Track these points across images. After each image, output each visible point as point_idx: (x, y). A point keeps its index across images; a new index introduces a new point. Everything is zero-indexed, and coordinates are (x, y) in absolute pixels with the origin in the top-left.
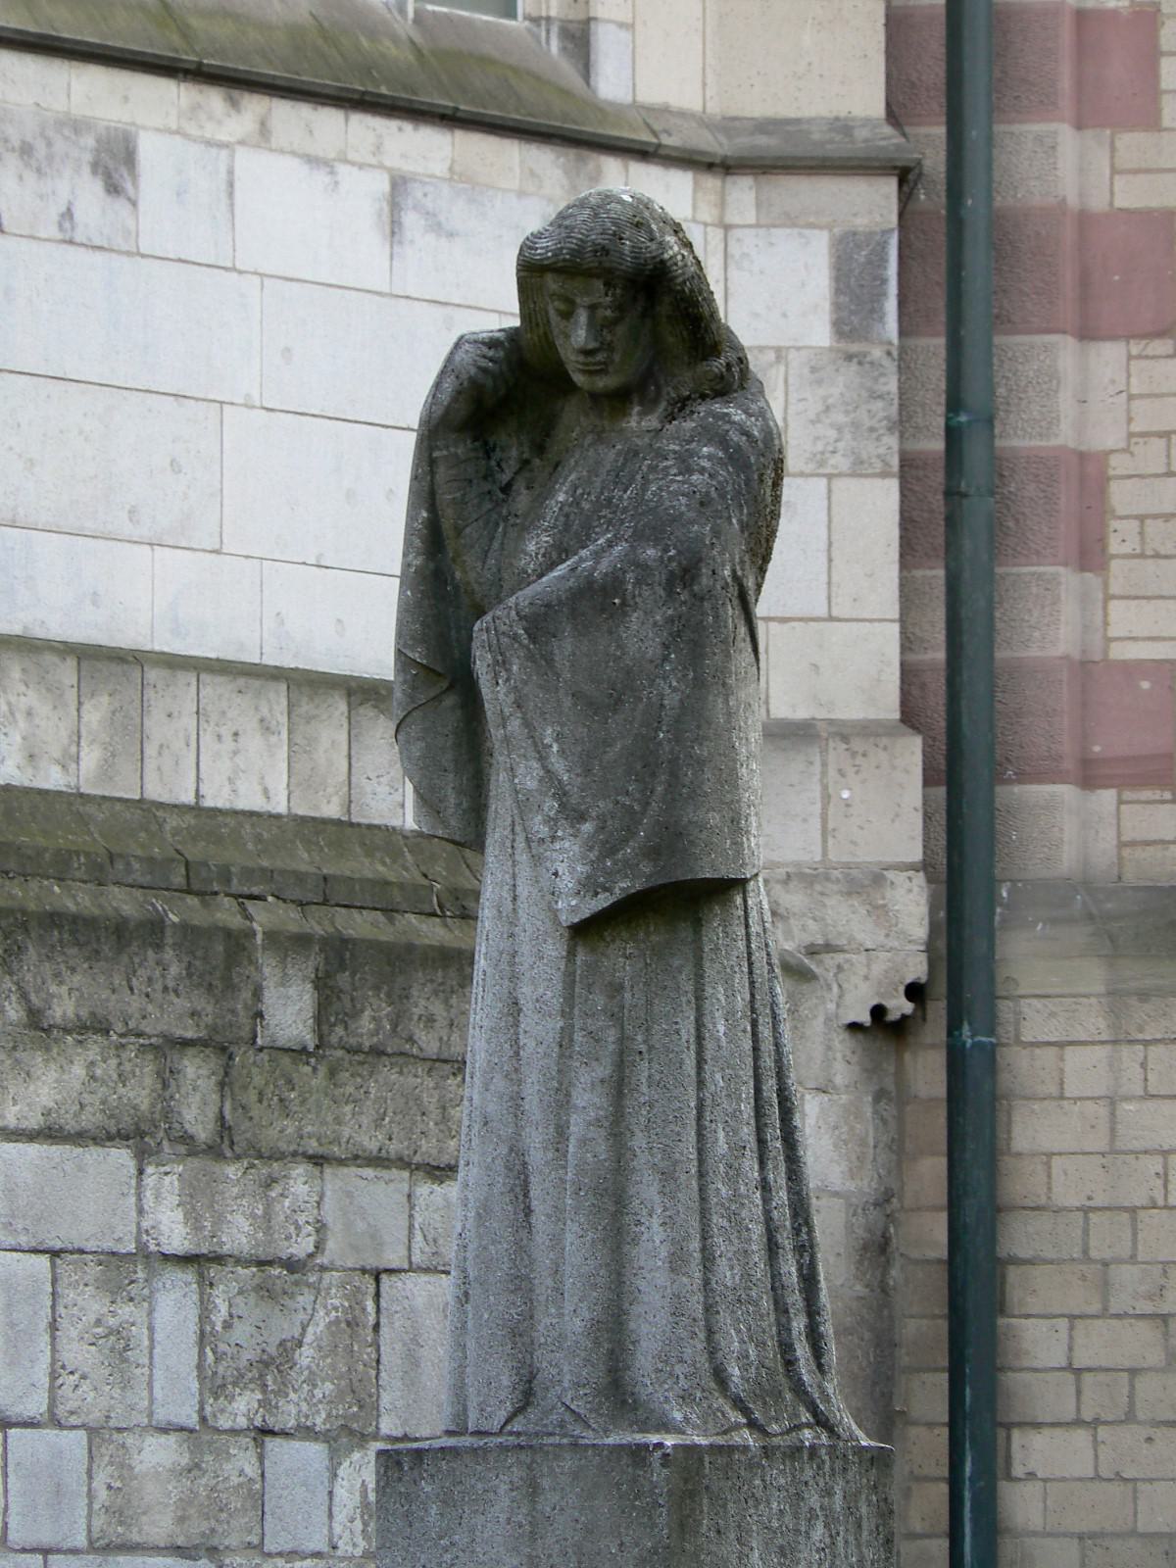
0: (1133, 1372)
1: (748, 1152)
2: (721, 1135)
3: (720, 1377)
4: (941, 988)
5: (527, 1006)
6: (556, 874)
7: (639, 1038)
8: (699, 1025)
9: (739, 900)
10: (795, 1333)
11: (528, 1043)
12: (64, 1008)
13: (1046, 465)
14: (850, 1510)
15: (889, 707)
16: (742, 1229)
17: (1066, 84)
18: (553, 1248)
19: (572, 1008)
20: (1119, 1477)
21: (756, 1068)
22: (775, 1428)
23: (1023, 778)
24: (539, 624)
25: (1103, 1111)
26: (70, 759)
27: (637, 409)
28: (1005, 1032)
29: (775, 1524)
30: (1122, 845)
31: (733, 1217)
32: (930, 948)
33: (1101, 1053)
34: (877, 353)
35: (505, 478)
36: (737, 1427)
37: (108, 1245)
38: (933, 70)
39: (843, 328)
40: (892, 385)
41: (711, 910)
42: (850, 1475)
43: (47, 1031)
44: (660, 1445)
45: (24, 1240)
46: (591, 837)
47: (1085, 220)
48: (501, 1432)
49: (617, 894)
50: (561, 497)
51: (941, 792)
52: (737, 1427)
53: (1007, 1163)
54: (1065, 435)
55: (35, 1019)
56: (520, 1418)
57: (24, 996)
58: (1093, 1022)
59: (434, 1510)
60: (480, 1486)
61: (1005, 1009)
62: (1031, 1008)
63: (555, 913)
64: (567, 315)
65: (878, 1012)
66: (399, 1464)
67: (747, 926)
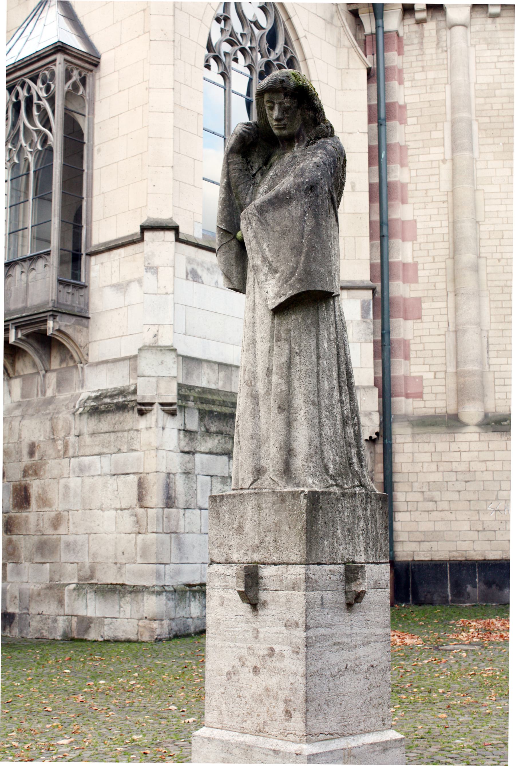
0: (417, 502)
1: (336, 389)
2: (326, 383)
3: (326, 469)
4: (382, 433)
5: (258, 340)
6: (267, 292)
7: (297, 348)
8: (318, 344)
9: (332, 303)
10: (353, 453)
11: (259, 353)
12: (213, 429)
13: (399, 341)
14: (373, 516)
15: (372, 383)
16: (334, 416)
17: (401, 275)
18: (267, 423)
19: (273, 339)
20: (415, 521)
21: (338, 361)
22: (346, 486)
23: (396, 396)
24: (262, 210)
25: (411, 455)
26: (216, 383)
27: (297, 144)
28: (393, 441)
29: (346, 520)
30: (414, 408)
31: (330, 411)
32: (380, 425)
33: (410, 445)
34: (369, 321)
35: (254, 172)
36: (332, 485)
37: (222, 475)
38: (378, 273)
39: (363, 317)
40: (372, 326)
41: (322, 304)
42: (373, 504)
43: (210, 433)
44: (303, 492)
45: (205, 473)
46: (279, 278)
47: (405, 300)
48: (249, 489)
49: (288, 296)
50: (271, 174)
51: (381, 399)
52: (332, 485)
53: (394, 465)
54: (402, 336)
55: (207, 431)
56: (256, 483)
57: (205, 426)
58: (409, 439)
59: (227, 516)
60: (242, 507)
61: (393, 437)
62: (397, 436)
63: (266, 305)
64: (272, 109)
65: (371, 437)
66: (216, 500)
67: (335, 312)
